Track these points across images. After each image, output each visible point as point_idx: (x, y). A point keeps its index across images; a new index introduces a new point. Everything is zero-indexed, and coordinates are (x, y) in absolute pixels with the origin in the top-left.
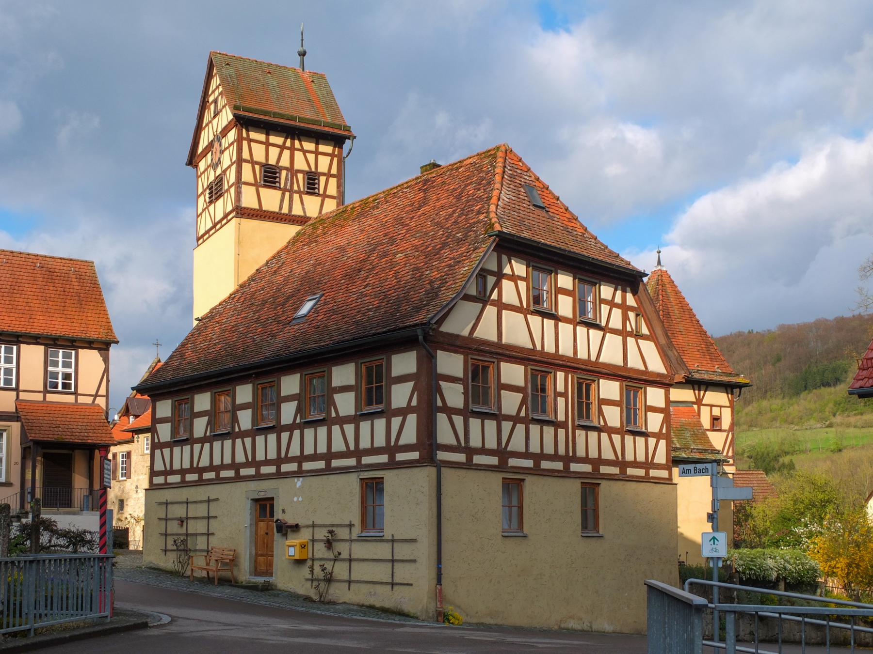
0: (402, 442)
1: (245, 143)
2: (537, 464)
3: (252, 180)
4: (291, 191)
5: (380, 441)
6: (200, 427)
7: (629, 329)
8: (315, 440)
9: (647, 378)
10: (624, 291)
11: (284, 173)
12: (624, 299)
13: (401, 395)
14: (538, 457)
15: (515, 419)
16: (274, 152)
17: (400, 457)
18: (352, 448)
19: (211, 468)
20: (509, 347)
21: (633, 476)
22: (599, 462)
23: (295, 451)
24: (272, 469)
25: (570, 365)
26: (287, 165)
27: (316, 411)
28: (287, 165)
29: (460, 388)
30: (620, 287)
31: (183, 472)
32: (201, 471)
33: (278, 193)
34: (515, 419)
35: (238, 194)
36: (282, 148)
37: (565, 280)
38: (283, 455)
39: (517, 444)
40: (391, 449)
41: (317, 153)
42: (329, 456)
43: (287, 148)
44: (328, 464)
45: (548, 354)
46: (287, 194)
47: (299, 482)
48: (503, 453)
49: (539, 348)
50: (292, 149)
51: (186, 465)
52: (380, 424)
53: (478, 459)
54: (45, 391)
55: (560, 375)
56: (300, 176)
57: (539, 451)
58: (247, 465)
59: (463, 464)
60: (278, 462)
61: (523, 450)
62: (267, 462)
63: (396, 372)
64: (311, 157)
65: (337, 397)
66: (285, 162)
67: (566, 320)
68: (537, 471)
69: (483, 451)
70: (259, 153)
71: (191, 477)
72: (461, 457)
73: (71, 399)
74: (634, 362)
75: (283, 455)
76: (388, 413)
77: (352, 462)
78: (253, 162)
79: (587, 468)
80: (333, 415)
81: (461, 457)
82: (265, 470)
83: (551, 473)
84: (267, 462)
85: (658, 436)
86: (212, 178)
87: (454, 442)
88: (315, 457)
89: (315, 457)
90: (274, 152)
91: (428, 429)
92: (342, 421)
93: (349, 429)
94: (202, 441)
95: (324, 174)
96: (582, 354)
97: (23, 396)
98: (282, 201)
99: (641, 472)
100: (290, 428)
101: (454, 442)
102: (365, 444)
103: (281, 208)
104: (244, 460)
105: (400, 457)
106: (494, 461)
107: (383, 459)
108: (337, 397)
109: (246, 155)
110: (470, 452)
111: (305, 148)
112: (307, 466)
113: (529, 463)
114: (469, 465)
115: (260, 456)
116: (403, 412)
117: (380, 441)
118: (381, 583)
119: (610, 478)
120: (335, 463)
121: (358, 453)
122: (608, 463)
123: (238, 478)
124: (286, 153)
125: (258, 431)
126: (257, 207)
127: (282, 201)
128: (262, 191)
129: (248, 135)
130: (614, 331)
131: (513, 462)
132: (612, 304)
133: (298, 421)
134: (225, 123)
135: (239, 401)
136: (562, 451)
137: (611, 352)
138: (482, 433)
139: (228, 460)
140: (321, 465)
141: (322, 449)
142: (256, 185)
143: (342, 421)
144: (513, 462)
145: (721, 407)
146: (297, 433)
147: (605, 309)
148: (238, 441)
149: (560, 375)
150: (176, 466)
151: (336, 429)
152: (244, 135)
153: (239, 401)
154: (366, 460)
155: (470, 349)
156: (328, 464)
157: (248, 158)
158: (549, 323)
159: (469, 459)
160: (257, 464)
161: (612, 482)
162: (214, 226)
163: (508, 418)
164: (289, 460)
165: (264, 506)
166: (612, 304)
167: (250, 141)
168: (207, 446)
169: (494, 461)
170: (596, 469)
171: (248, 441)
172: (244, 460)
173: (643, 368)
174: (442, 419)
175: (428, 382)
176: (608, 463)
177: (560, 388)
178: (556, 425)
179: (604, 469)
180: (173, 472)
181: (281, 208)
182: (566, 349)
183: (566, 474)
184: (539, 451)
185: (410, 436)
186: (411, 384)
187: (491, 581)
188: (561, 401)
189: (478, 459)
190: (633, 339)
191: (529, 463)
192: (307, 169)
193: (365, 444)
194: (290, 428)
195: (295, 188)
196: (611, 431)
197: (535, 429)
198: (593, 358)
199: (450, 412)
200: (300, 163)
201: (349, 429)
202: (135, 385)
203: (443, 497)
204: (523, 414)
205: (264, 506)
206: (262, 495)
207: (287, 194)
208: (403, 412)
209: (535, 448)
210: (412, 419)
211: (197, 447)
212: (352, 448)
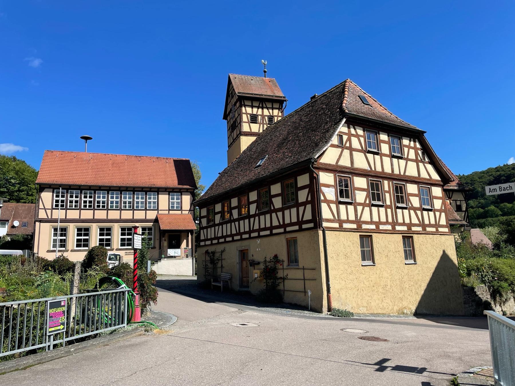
0: (304, 219)
2: (377, 227)
5: (294, 220)
6: (218, 219)
7: (419, 159)
8: (265, 221)
9: (431, 182)
10: (415, 142)
11: (260, 117)
13: (303, 196)
14: (378, 223)
15: (364, 205)
17: (304, 226)
18: (282, 223)
19: (223, 237)
20: (357, 169)
21: (429, 232)
22: (410, 225)
23: (256, 227)
24: (247, 236)
25: (390, 177)
26: (261, 114)
27: (265, 206)
28: (261, 114)
29: (333, 190)
30: (412, 139)
31: (211, 239)
32: (218, 238)
34: (364, 205)
37: (384, 137)
38: (251, 229)
39: (366, 217)
40: (300, 223)
42: (272, 228)
44: (271, 232)
46: (261, 125)
47: (259, 241)
48: (358, 222)
49: (373, 169)
51: (213, 236)
52: (294, 210)
53: (345, 226)
54: (169, 210)
56: (266, 118)
58: (236, 234)
59: (338, 228)
60: (250, 232)
61: (370, 220)
62: (245, 233)
63: (300, 185)
65: (274, 200)
67: (386, 155)
68: (378, 231)
69: (348, 221)
71: (215, 241)
72: (336, 225)
73: (180, 212)
74: (424, 175)
75: (251, 229)
76: (298, 205)
77: (282, 230)
78: (246, 113)
79: (405, 228)
80: (272, 208)
81: (336, 225)
82: (244, 236)
83: (385, 232)
84: (245, 233)
85: (440, 211)
86: (232, 122)
87: (332, 217)
88: (265, 229)
89: (265, 229)
92: (276, 211)
93: (280, 214)
94: (218, 225)
96: (396, 172)
97: (160, 212)
98: (259, 128)
99: (434, 230)
100: (254, 216)
101: (332, 217)
102: (287, 221)
103: (259, 131)
104: (235, 233)
105: (304, 226)
106: (354, 226)
107: (296, 228)
108: (274, 200)
110: (341, 222)
111: (268, 106)
112: (262, 233)
113: (373, 227)
114: (341, 229)
115: (242, 230)
116: (304, 204)
117: (294, 220)
119: (418, 233)
120: (275, 231)
121: (284, 226)
122: (415, 225)
123: (233, 241)
127: (259, 128)
129: (244, 103)
130: (412, 160)
131: (364, 226)
132: (409, 147)
133: (257, 212)
134: (235, 100)
135: (232, 206)
136: (390, 220)
137: (412, 171)
138: (347, 212)
139: (229, 233)
140: (268, 232)
141: (268, 225)
142: (248, 122)
143: (276, 211)
144: (364, 226)
145: (460, 201)
146: (257, 218)
147: (406, 150)
148: (233, 224)
149: (386, 182)
150: (209, 237)
151: (274, 215)
153: (232, 206)
154: (289, 229)
155: (336, 171)
156: (271, 232)
158: (377, 157)
159: (341, 226)
160: (240, 234)
161: (419, 235)
163: (360, 204)
164: (254, 231)
165: (243, 254)
166: (409, 147)
168: (221, 227)
169: (354, 226)
170: (409, 228)
172: (235, 233)
173: (428, 177)
174: (324, 206)
175: (314, 187)
176: (415, 225)
177: (386, 188)
178: (387, 207)
179: (414, 229)
180: (208, 240)
181: (259, 131)
182: (388, 170)
183: (394, 232)
185: (308, 216)
186: (307, 190)
187: (358, 290)
188: (387, 195)
189: (345, 226)
191: (373, 227)
193: (287, 221)
194: (254, 216)
196: (415, 209)
197: (374, 209)
198: (402, 173)
199: (328, 202)
201: (280, 214)
202: (446, 252)
203: (327, 246)
204: (367, 202)
205: (243, 254)
206: (243, 248)
207: (261, 125)
208: (304, 204)
209: (376, 219)
210: (309, 207)
211: (217, 228)
212: (282, 223)
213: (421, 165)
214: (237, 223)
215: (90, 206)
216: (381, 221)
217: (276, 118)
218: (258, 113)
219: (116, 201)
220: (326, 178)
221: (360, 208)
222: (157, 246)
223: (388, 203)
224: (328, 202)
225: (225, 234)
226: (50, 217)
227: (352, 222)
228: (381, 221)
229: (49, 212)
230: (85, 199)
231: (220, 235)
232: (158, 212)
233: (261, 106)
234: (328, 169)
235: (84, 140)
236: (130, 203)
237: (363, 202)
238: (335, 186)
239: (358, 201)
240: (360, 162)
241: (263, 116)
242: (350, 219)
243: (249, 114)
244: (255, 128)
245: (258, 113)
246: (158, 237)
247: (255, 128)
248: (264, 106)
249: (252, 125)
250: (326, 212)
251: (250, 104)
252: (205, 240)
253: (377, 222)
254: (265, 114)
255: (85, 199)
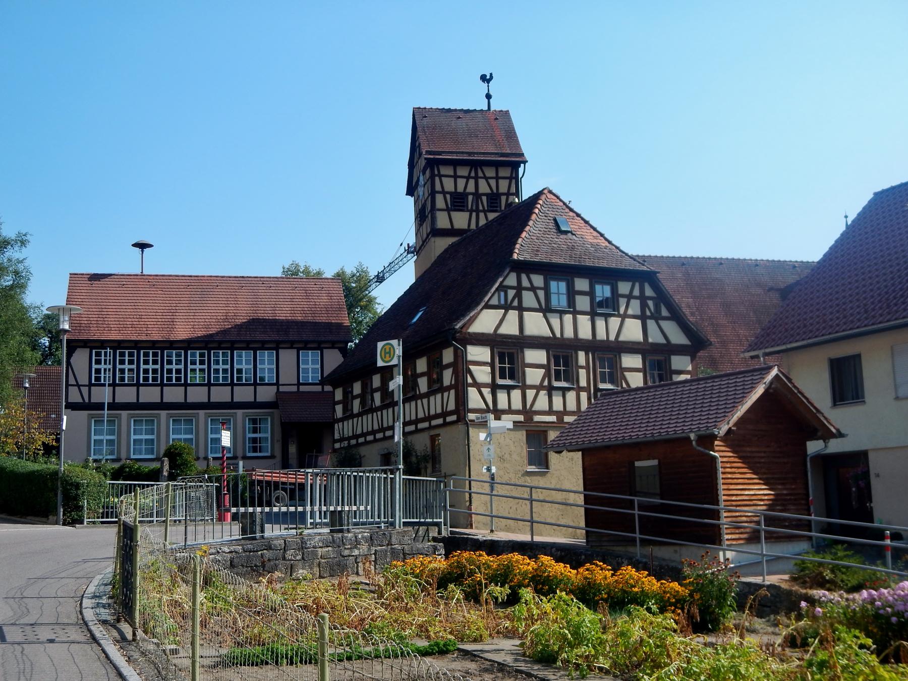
0: (449, 409)
1: (437, 179)
3: (444, 207)
4: (478, 211)
11: (470, 198)
12: (642, 290)
13: (448, 377)
15: (538, 388)
16: (461, 183)
25: (593, 347)
26: (473, 191)
28: (473, 191)
33: (467, 214)
35: (434, 220)
36: (468, 178)
39: (542, 403)
41: (497, 178)
43: (472, 178)
45: (568, 339)
46: (474, 214)
50: (476, 178)
55: (581, 356)
56: (484, 198)
57: (562, 409)
64: (493, 183)
66: (471, 188)
70: (449, 184)
78: (443, 192)
90: (461, 183)
91: (461, 400)
95: (504, 194)
97: (282, 389)
103: (469, 225)
109: (438, 187)
111: (488, 175)
113: (553, 418)
116: (448, 389)
118: (575, 492)
124: (472, 182)
125: (431, 393)
126: (450, 227)
128: (453, 214)
131: (537, 418)
142: (448, 210)
144: (537, 418)
152: (436, 172)
157: (490, 181)
162: (424, 242)
167: (440, 176)
171: (425, 401)
173: (664, 342)
174: (472, 392)
175: (461, 366)
181: (469, 225)
184: (562, 409)
188: (582, 373)
190: (653, 321)
191: (553, 418)
192: (489, 191)
195: (481, 208)
199: (478, 386)
200: (484, 188)
204: (546, 383)
207: (474, 214)
210: (453, 392)
213: (651, 324)
214: (379, 413)
215: (155, 379)
216: (568, 409)
217: (503, 198)
218: (468, 190)
219: (195, 364)
220: (478, 353)
221: (530, 394)
222: (278, 453)
223: (583, 383)
224: (478, 386)
225: (365, 431)
226: (87, 400)
227: (517, 412)
228: (568, 409)
229: (85, 390)
230: (146, 367)
231: (359, 432)
232: (278, 389)
233: (473, 174)
234: (480, 340)
235: (138, 250)
236: (225, 371)
237: (538, 383)
238: (492, 365)
239: (529, 382)
240: (536, 325)
241: (477, 195)
242: (514, 407)
243: (448, 193)
244: (461, 220)
245: (468, 190)
246: (278, 436)
247: (461, 220)
248: (480, 174)
249: (455, 215)
250: (474, 399)
251: (452, 173)
252: (341, 440)
253: (560, 412)
254: (481, 191)
255: (146, 367)
